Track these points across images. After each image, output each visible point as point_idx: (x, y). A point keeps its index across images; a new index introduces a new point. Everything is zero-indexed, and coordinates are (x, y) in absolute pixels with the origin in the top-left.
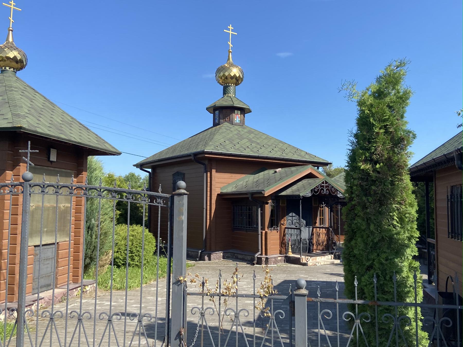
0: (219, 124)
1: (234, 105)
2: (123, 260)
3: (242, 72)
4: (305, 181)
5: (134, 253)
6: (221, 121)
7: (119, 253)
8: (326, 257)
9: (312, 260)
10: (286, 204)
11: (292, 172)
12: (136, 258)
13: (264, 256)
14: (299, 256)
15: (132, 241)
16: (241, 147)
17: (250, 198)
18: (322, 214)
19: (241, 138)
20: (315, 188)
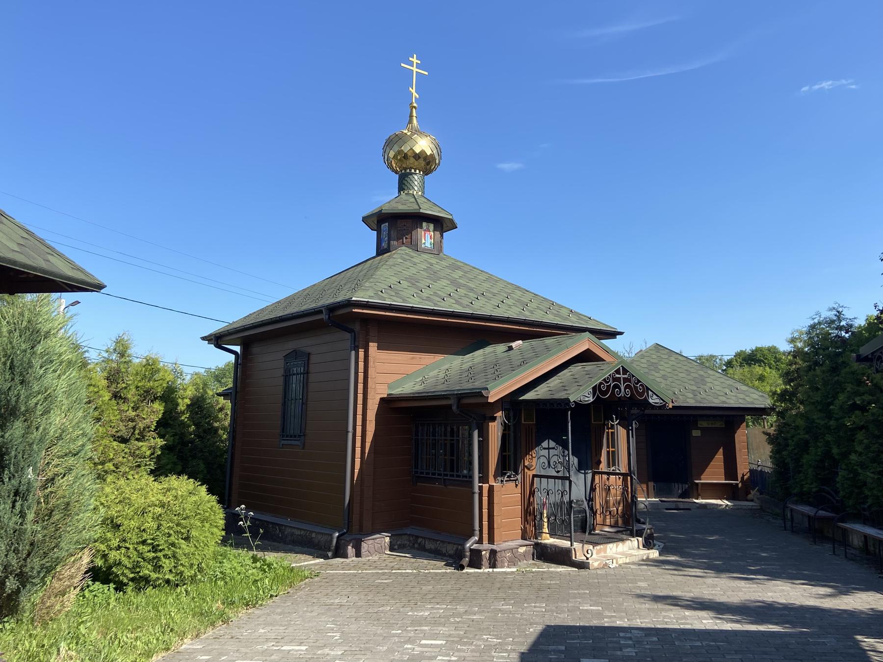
0: (388, 250)
1: (421, 211)
2: (132, 570)
3: (438, 147)
4: (576, 369)
5: (161, 551)
6: (394, 243)
7: (123, 551)
8: (628, 543)
9: (597, 553)
10: (536, 420)
11: (548, 348)
12: (167, 564)
13: (486, 545)
14: (566, 544)
15: (157, 518)
16: (435, 294)
17: (454, 408)
18: (613, 442)
19: (435, 276)
20: (601, 383)
